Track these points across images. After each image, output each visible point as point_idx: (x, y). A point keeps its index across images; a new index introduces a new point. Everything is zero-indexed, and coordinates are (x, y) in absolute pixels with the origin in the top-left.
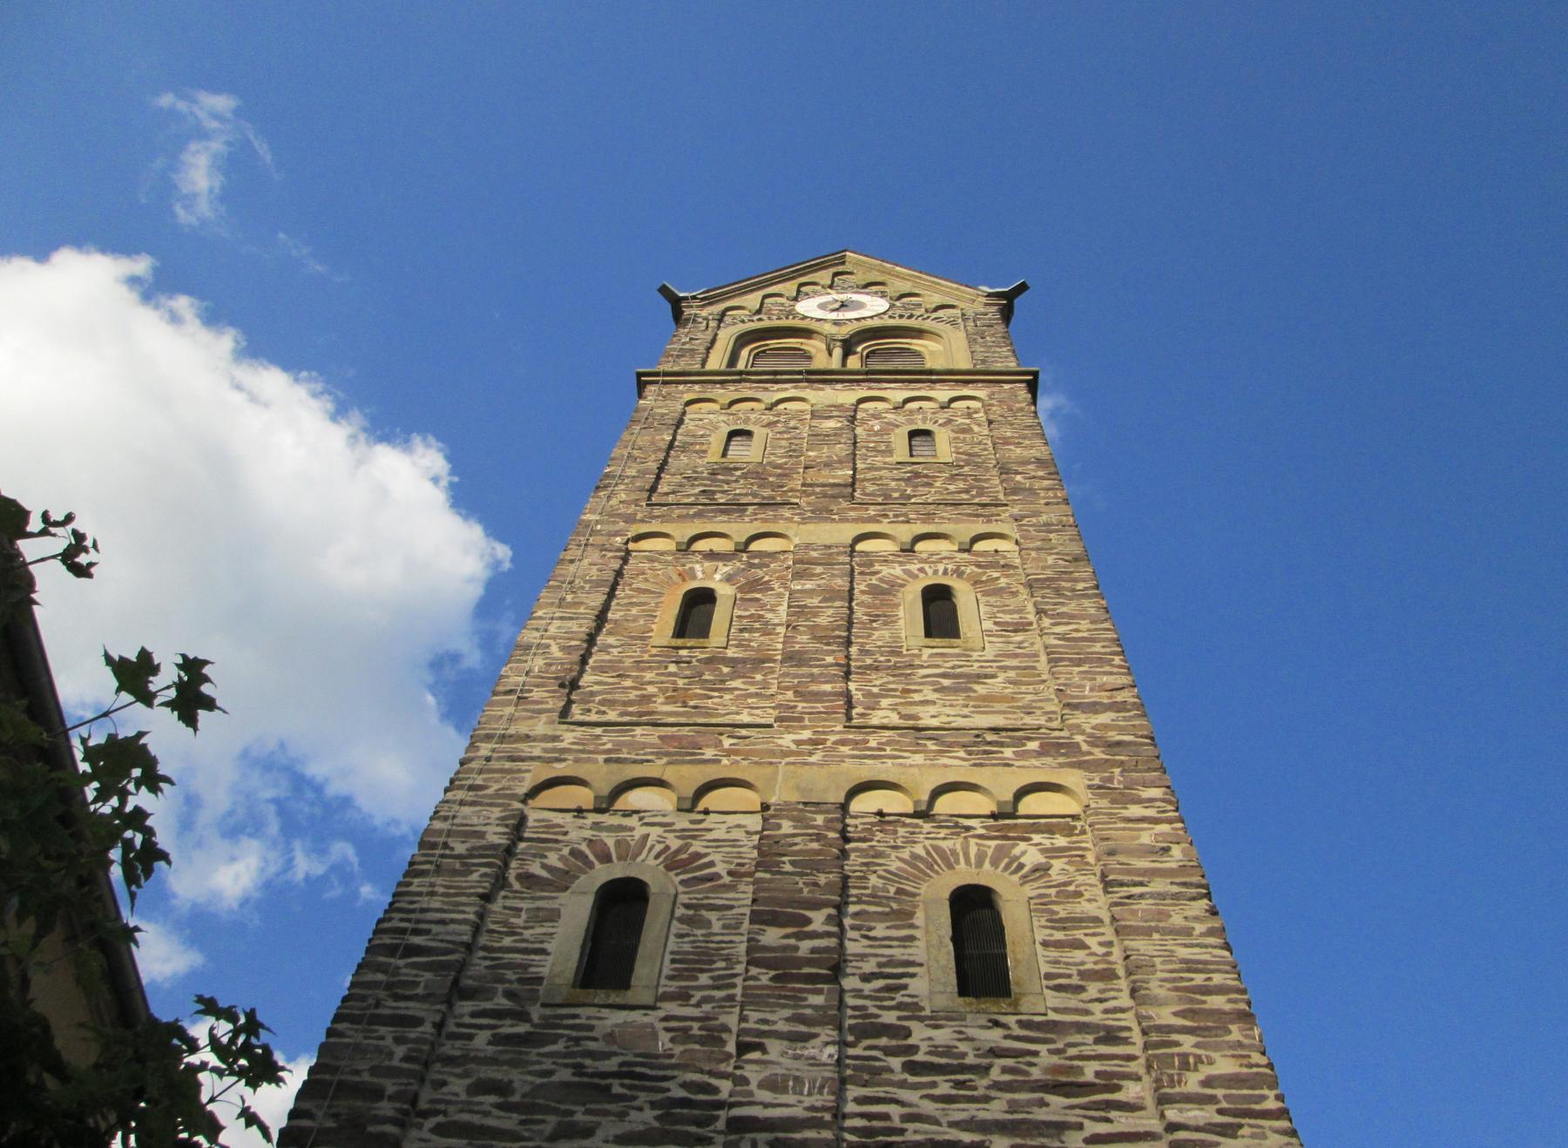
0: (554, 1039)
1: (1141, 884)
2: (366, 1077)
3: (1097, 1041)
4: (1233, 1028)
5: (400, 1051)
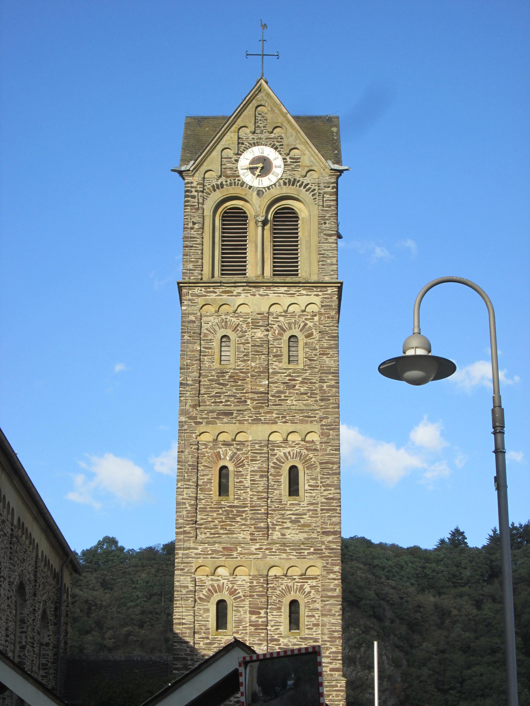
0: (215, 643)
2: (184, 656)
3: (313, 642)
4: (337, 640)
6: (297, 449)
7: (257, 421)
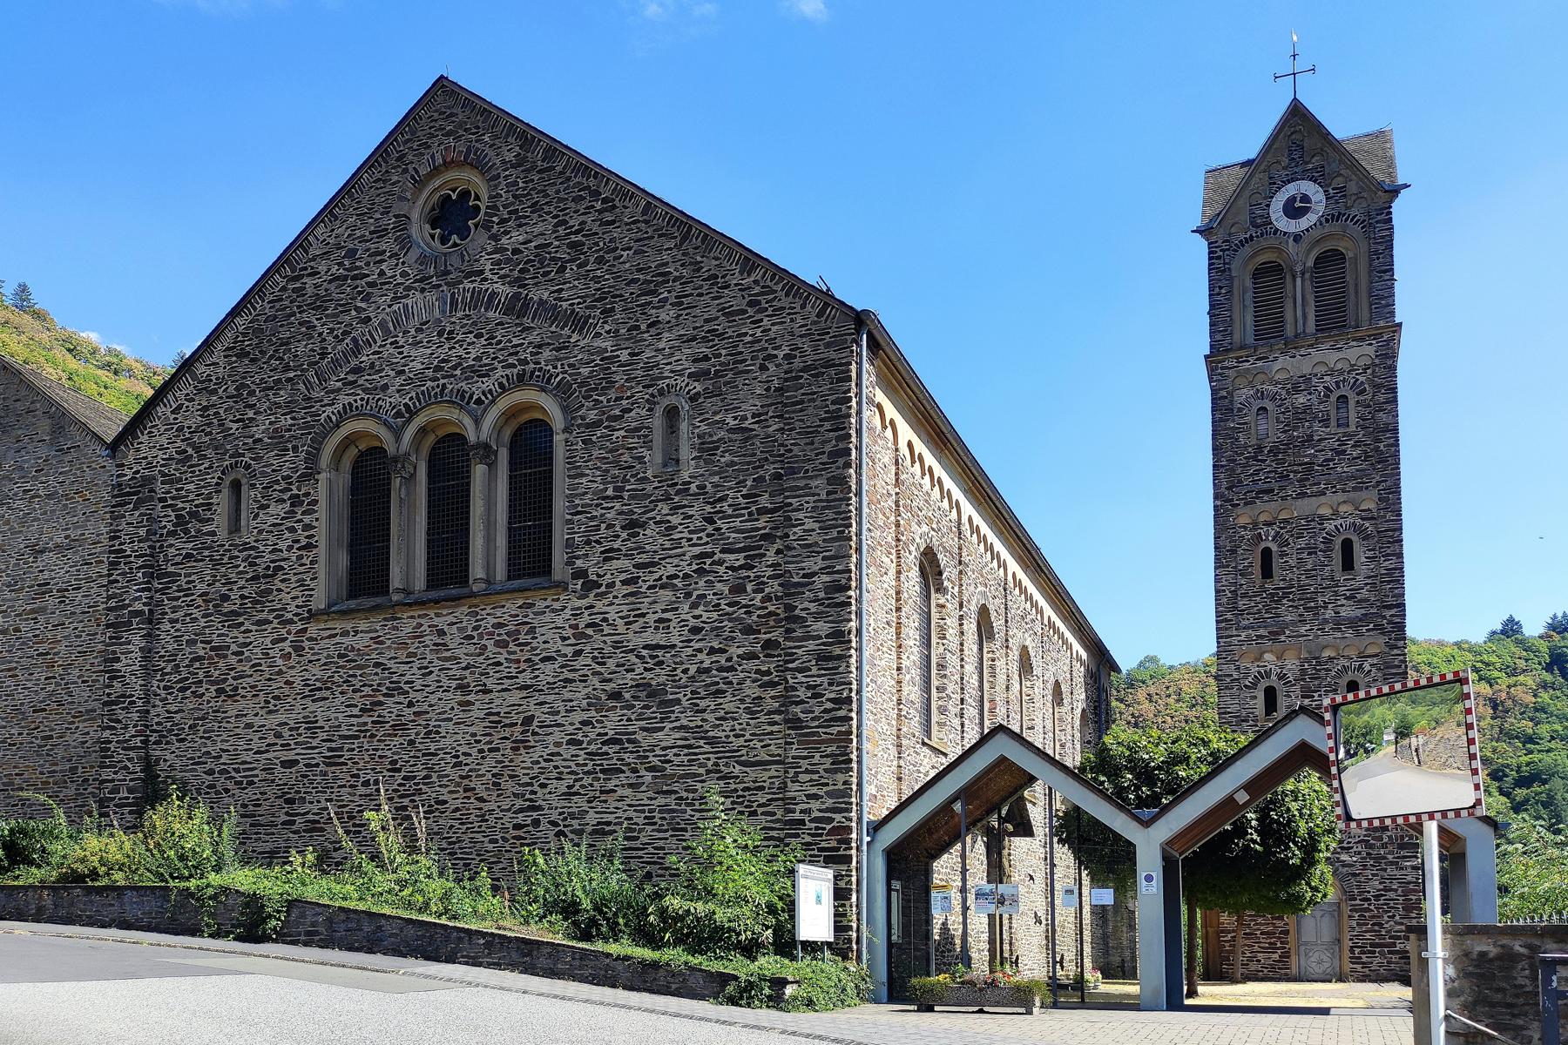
6: (1350, 520)
7: (1303, 495)
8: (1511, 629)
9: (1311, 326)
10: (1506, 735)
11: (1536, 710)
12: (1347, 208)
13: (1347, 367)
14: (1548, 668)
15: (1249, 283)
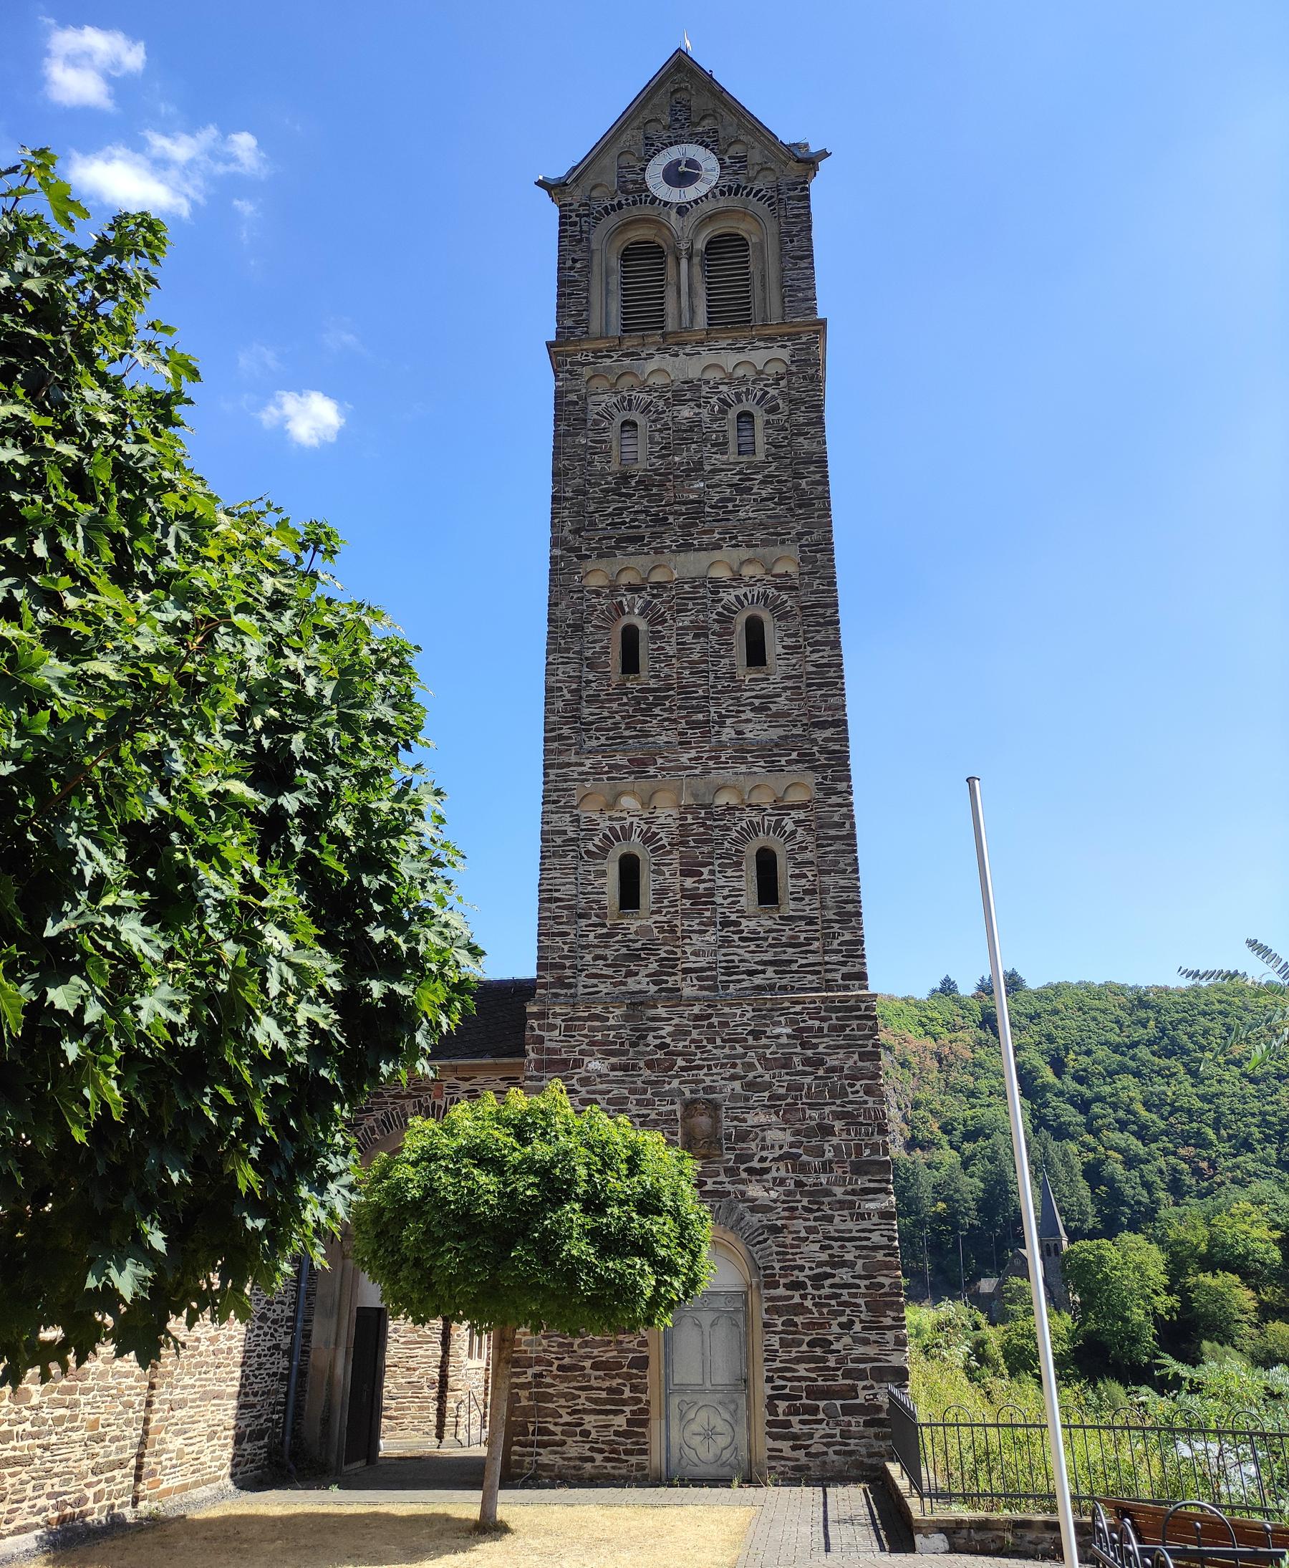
1: (831, 845)
5: (566, 947)
6: (759, 589)
7: (686, 547)
8: (947, 988)
9: (702, 320)
10: (951, 1088)
11: (975, 1065)
12: (749, 180)
13: (751, 375)
14: (981, 1026)
15: (615, 263)
